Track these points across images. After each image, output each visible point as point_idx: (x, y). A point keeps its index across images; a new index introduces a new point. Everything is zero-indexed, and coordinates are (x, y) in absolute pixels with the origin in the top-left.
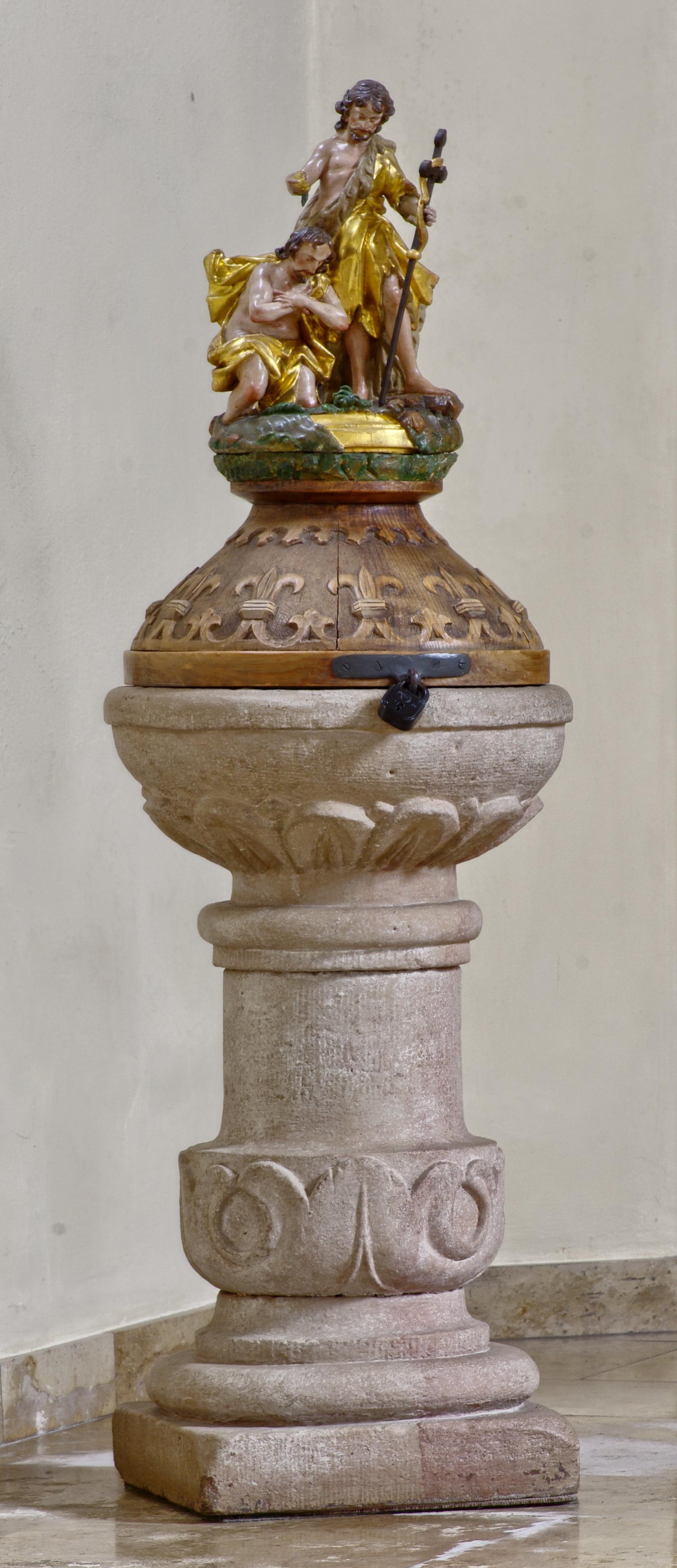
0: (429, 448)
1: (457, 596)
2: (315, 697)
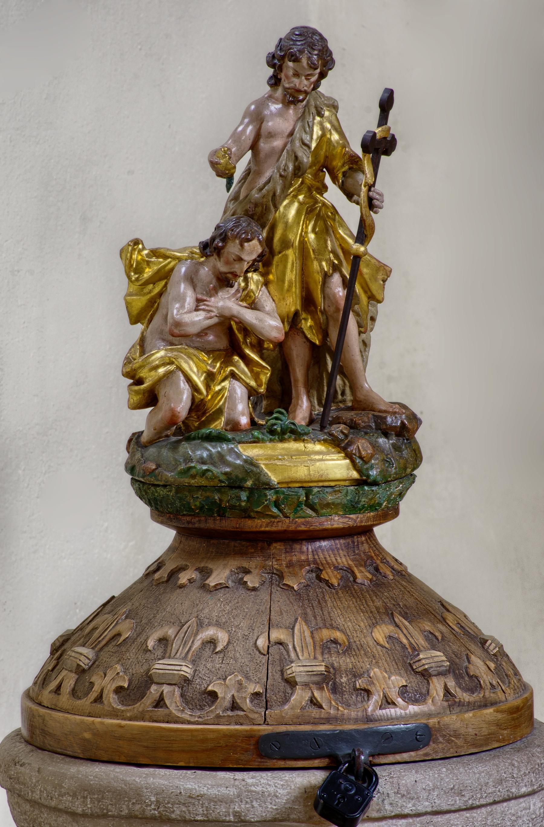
0: (379, 479)
1: (414, 649)
2: (237, 783)
